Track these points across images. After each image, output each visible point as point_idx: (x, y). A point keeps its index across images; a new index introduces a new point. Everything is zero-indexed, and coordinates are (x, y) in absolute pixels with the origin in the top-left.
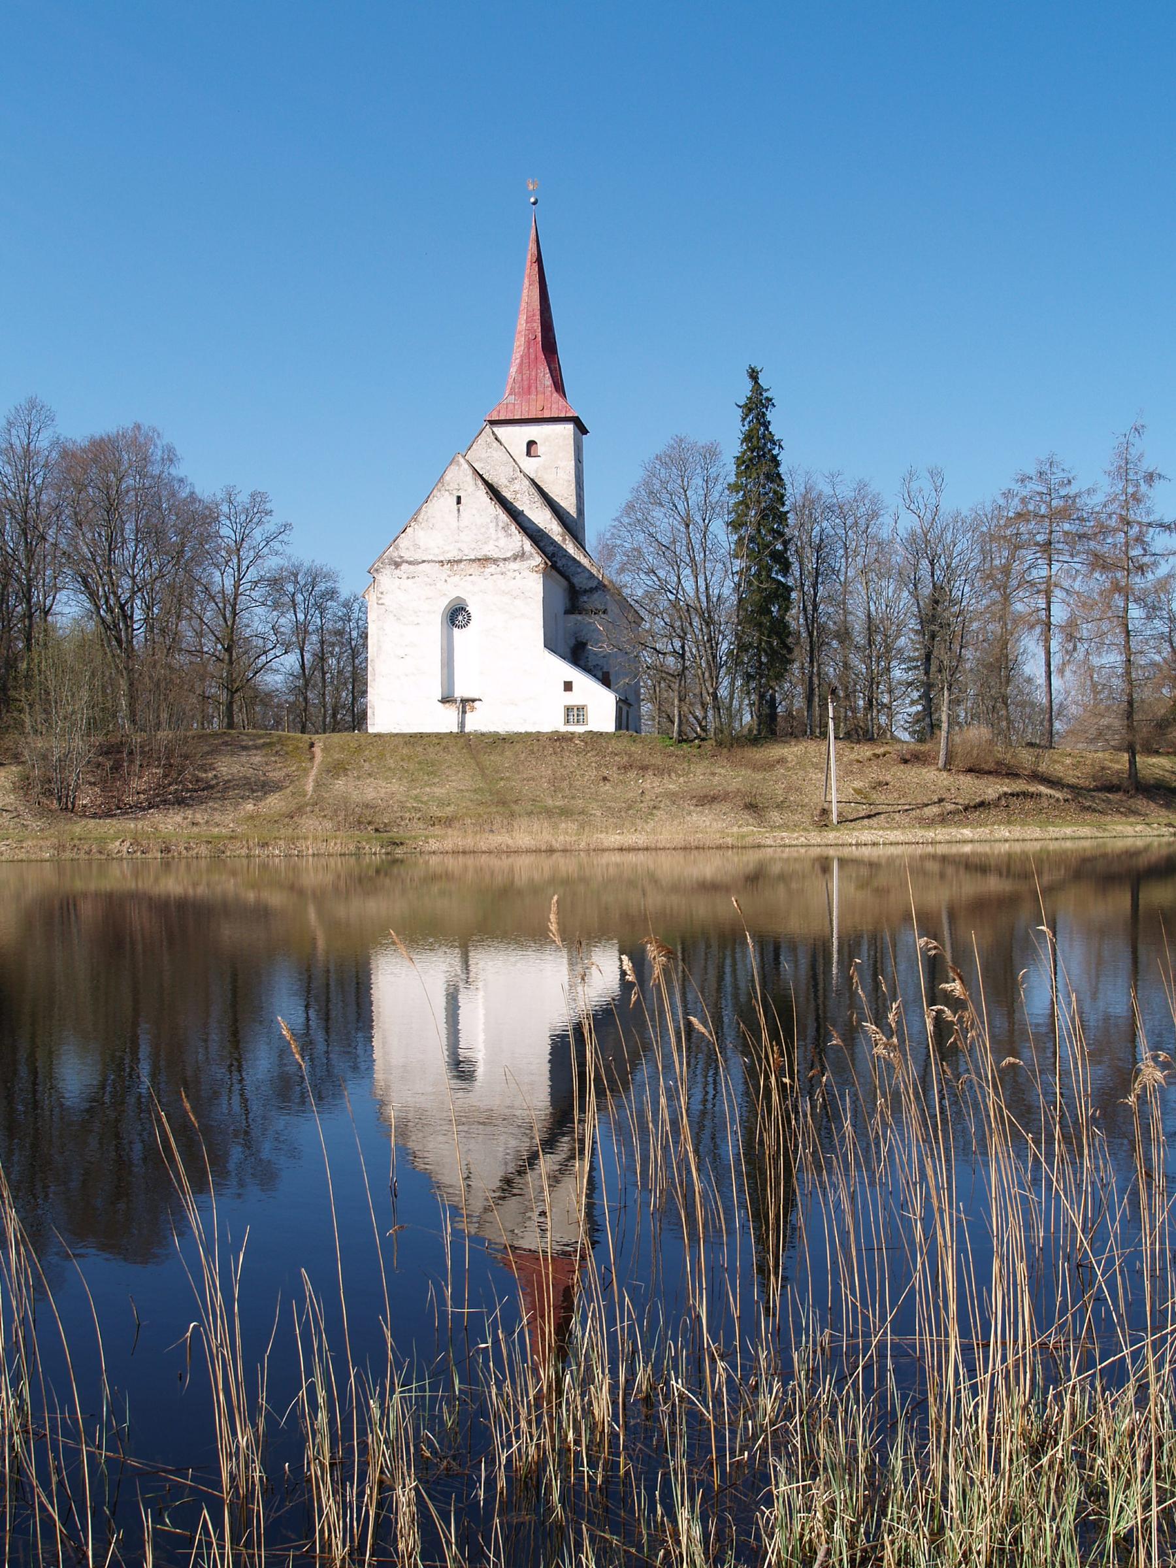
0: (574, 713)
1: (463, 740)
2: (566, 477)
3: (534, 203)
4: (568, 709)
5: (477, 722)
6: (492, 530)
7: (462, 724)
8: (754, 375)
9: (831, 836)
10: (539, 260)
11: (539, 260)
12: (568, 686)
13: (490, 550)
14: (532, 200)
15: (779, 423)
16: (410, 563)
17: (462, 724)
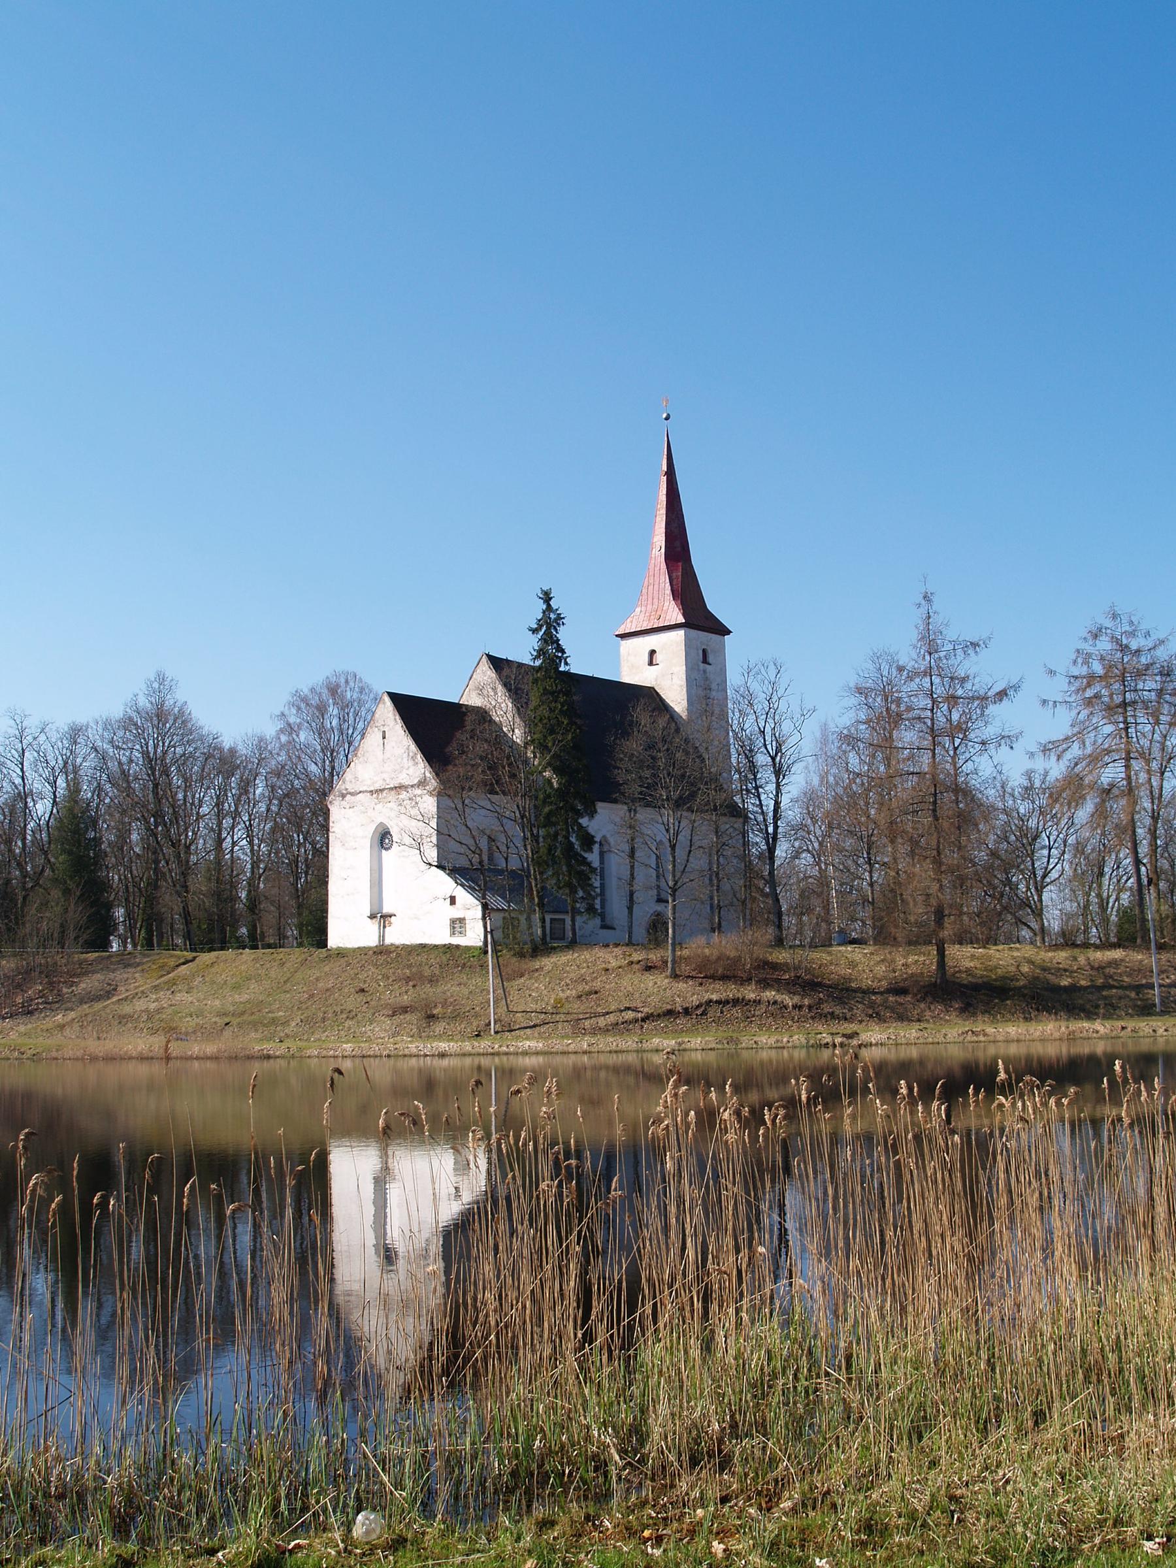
0: (457, 924)
1: (382, 951)
2: (679, 682)
3: (667, 418)
4: (453, 922)
5: (397, 935)
6: (405, 760)
7: (382, 937)
8: (547, 597)
9: (484, 1045)
10: (670, 474)
11: (670, 474)
12: (453, 900)
13: (404, 779)
14: (665, 416)
15: (564, 635)
16: (352, 794)
17: (382, 937)
